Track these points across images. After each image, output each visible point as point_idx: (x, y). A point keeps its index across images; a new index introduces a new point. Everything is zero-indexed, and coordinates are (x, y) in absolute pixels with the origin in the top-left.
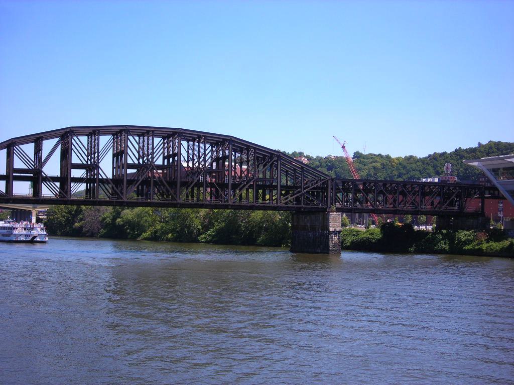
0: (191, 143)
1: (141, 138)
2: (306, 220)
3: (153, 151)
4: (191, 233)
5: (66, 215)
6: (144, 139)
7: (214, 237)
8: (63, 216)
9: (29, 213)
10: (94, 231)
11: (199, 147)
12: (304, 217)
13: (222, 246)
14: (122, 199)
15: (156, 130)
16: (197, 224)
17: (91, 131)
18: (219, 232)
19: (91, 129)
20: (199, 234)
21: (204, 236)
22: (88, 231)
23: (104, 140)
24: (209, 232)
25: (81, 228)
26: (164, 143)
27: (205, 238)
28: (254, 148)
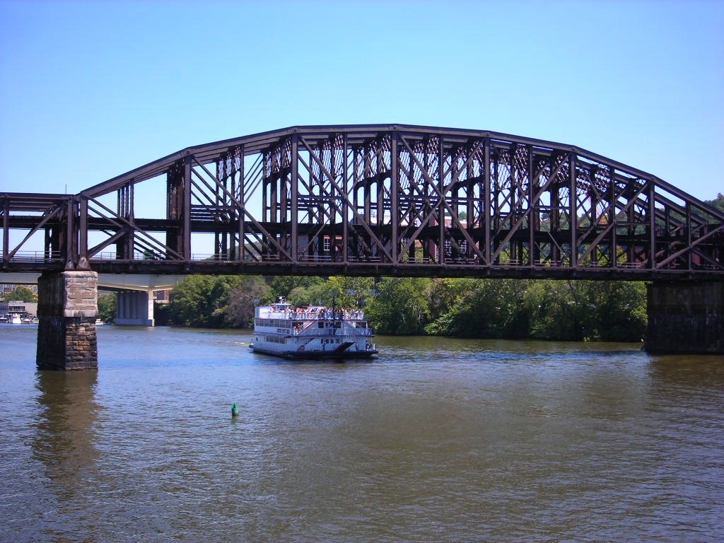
0: (317, 153)
1: (221, 162)
2: (680, 296)
3: (242, 190)
4: (411, 319)
5: (199, 297)
6: (225, 163)
7: (451, 326)
8: (195, 299)
9: (144, 296)
10: (244, 320)
11: (332, 156)
12: (674, 290)
13: (462, 340)
14: (390, 261)
15: (249, 140)
16: (421, 305)
17: (226, 150)
18: (459, 319)
19: (224, 145)
20: (426, 321)
21: (434, 325)
22: (234, 320)
23: (252, 161)
24: (441, 318)
25: (222, 316)
26: (264, 160)
27: (436, 328)
28: (438, 135)
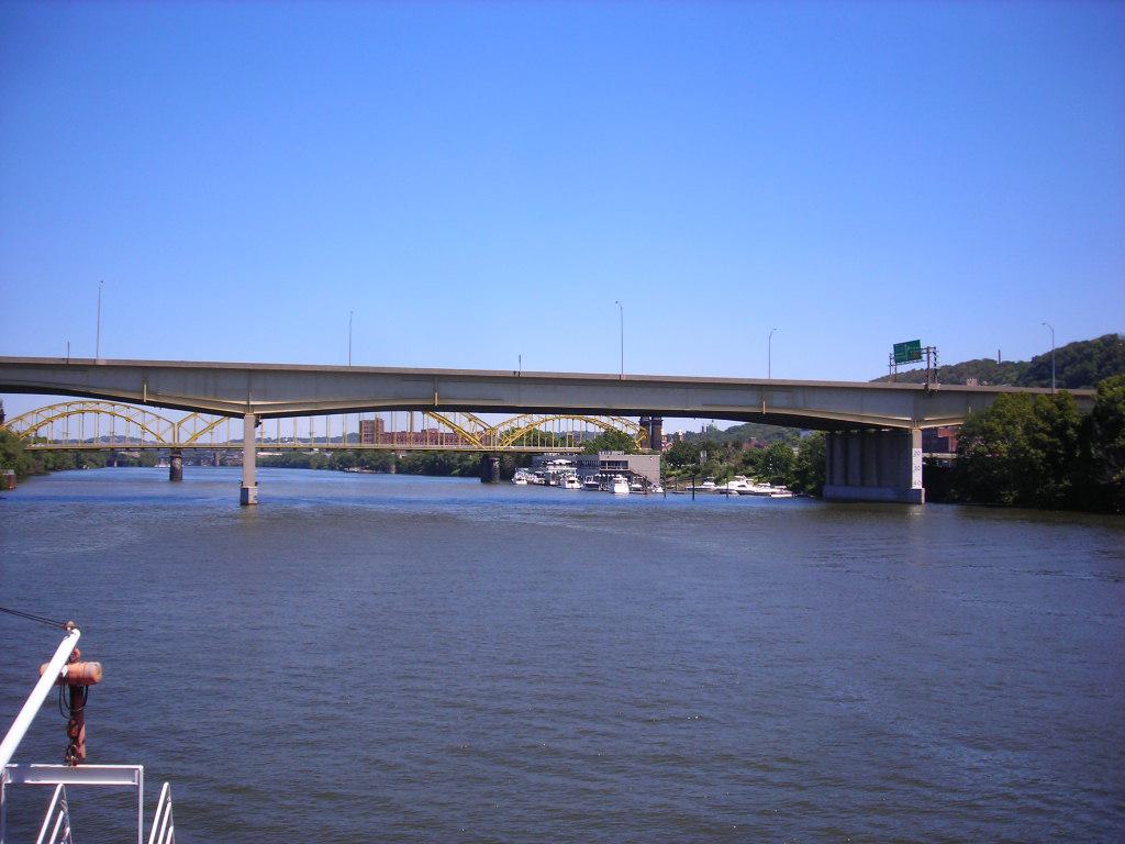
9: (901, 438)
